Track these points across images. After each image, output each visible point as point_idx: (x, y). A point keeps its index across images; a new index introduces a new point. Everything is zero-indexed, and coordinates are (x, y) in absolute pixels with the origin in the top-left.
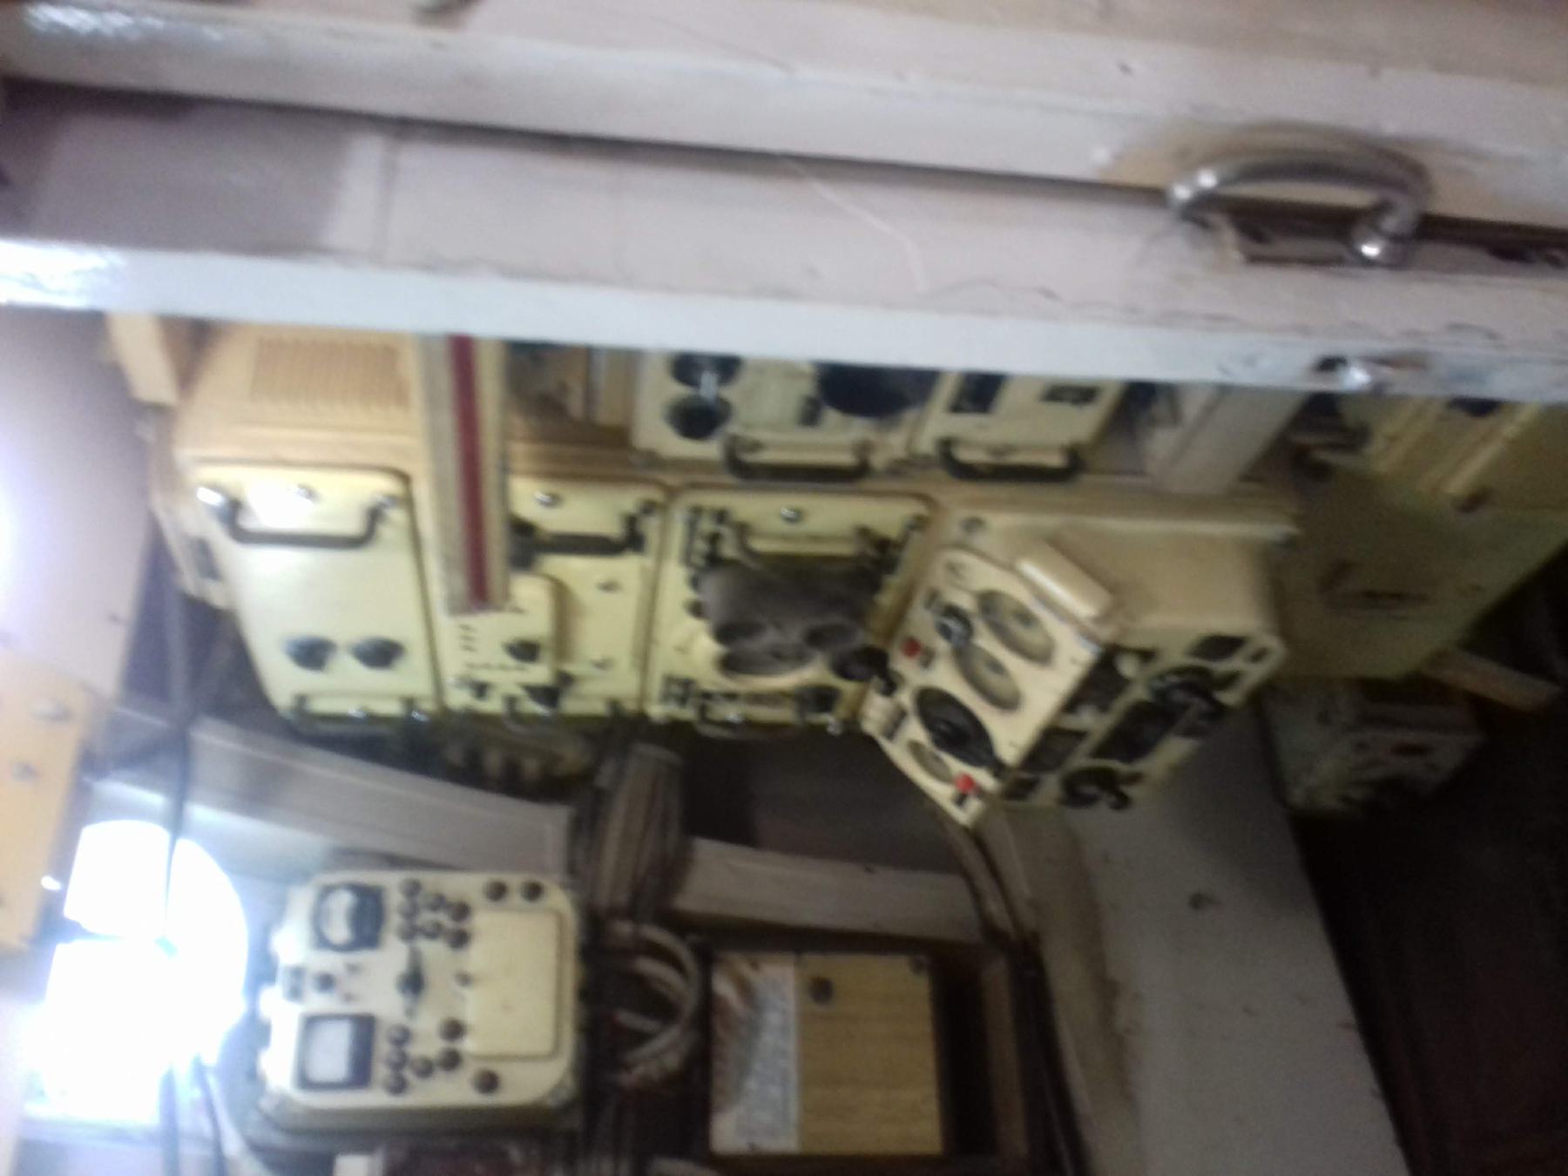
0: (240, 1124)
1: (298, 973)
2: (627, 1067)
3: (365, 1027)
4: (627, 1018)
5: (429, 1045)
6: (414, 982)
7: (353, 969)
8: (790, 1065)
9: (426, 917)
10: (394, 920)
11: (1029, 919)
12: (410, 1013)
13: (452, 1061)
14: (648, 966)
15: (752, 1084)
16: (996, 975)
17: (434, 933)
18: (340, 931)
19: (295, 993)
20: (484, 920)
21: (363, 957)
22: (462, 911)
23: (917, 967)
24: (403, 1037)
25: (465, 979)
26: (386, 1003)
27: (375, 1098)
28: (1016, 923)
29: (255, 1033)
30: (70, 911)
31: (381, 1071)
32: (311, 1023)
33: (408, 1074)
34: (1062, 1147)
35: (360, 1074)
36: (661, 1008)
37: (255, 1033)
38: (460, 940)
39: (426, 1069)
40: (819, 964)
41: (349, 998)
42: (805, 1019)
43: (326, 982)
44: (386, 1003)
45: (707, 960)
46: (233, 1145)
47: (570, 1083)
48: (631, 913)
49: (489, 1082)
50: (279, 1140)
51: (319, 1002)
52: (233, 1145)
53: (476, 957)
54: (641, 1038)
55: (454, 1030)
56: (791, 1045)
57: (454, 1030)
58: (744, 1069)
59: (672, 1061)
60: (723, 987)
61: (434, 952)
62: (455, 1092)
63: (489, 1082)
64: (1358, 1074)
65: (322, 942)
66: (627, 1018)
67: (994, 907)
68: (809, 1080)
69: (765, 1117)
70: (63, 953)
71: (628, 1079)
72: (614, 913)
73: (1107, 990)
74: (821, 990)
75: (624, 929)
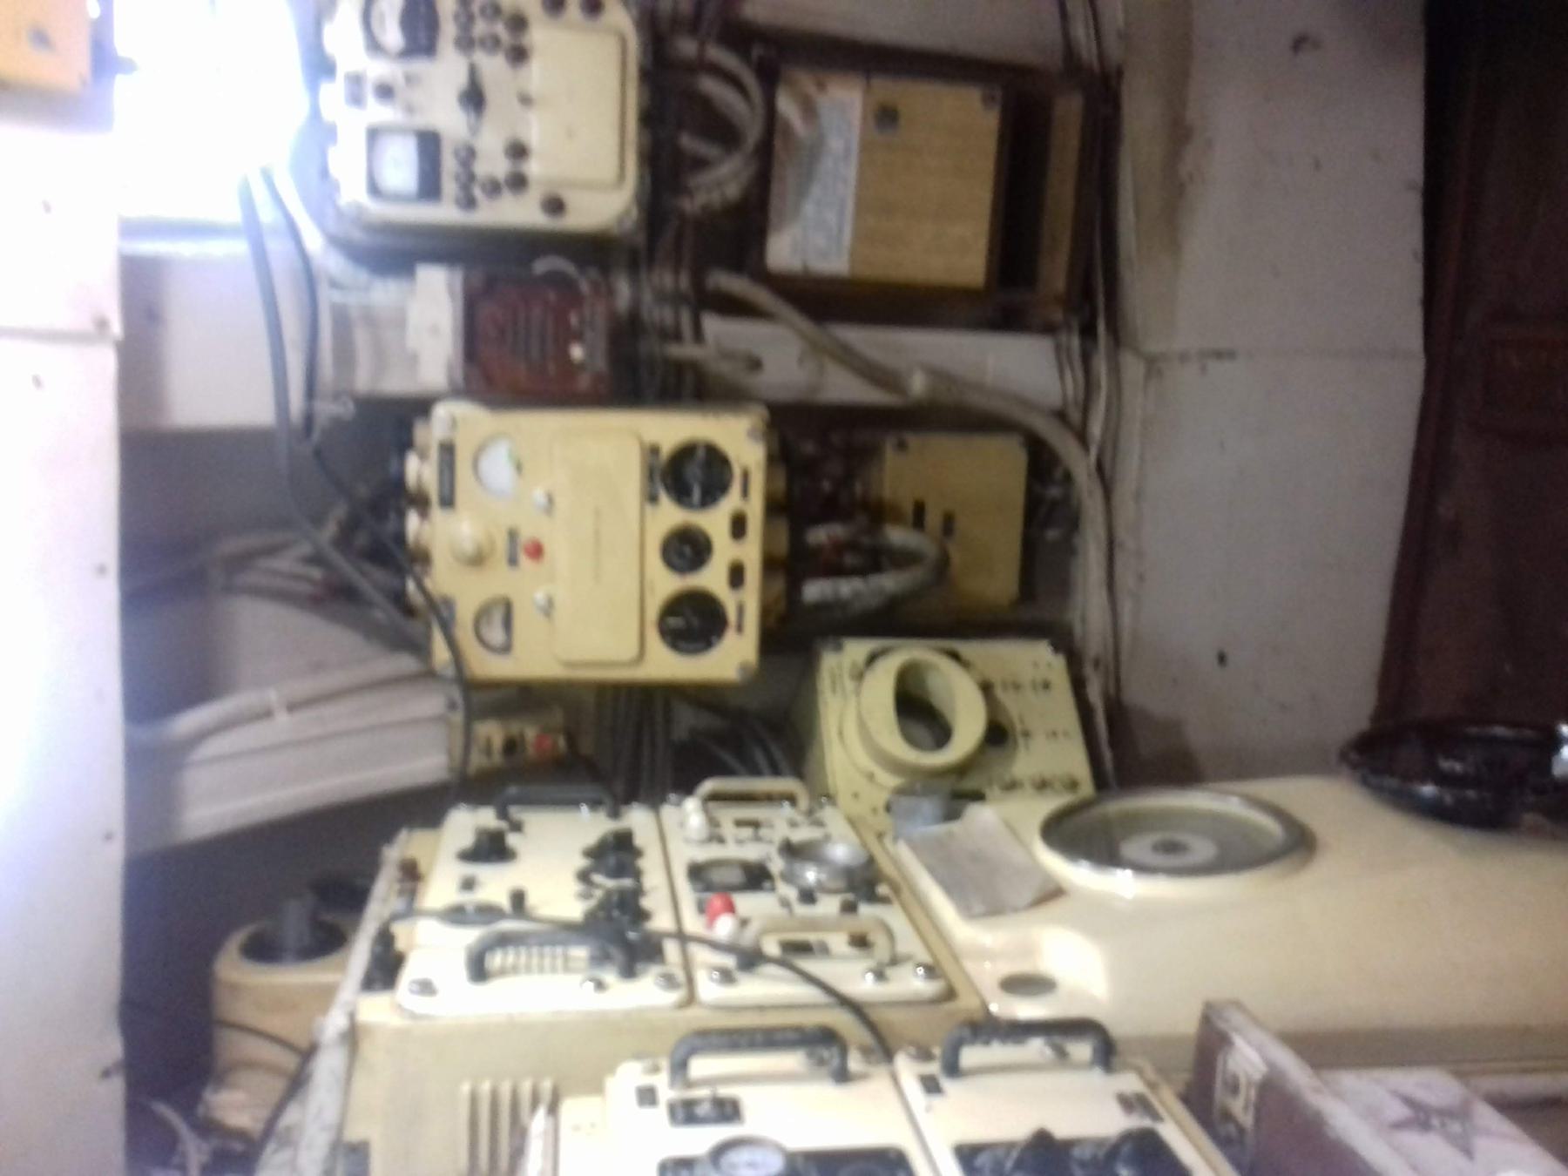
0: (318, 218)
1: (356, 81)
2: (688, 192)
3: (429, 144)
4: (689, 142)
5: (492, 163)
6: (474, 98)
7: (410, 80)
8: (848, 192)
9: (480, 28)
10: (449, 30)
11: (1114, 50)
12: (474, 130)
13: (518, 182)
14: (710, 86)
15: (809, 208)
16: (1069, 110)
17: (493, 44)
18: (393, 36)
19: (356, 99)
20: (541, 35)
21: (419, 66)
22: (519, 23)
23: (987, 100)
24: (468, 155)
25: (526, 100)
26: (449, 119)
27: (445, 213)
28: (1101, 56)
29: (320, 133)
30: (123, 44)
31: (449, 187)
32: (374, 135)
33: (477, 192)
34: (1107, 755)
35: (430, 187)
36: (724, 132)
37: (320, 133)
38: (519, 55)
39: (494, 188)
40: (888, 89)
41: (410, 109)
42: (865, 147)
43: (385, 92)
44: (449, 119)
45: (770, 77)
46: (314, 242)
47: (634, 213)
48: (694, 25)
49: (555, 206)
50: (358, 235)
51: (379, 112)
52: (314, 242)
53: (536, 74)
54: (701, 164)
55: (518, 151)
56: (851, 172)
57: (518, 151)
58: (802, 192)
59: (733, 191)
60: (786, 105)
61: (493, 66)
62: (521, 213)
63: (555, 206)
64: (1411, 236)
65: (374, 45)
66: (688, 142)
67: (1081, 32)
68: (862, 206)
69: (819, 240)
70: (121, 84)
71: (691, 205)
72: (676, 22)
73: (1179, 133)
74: (886, 116)
75: (687, 47)
